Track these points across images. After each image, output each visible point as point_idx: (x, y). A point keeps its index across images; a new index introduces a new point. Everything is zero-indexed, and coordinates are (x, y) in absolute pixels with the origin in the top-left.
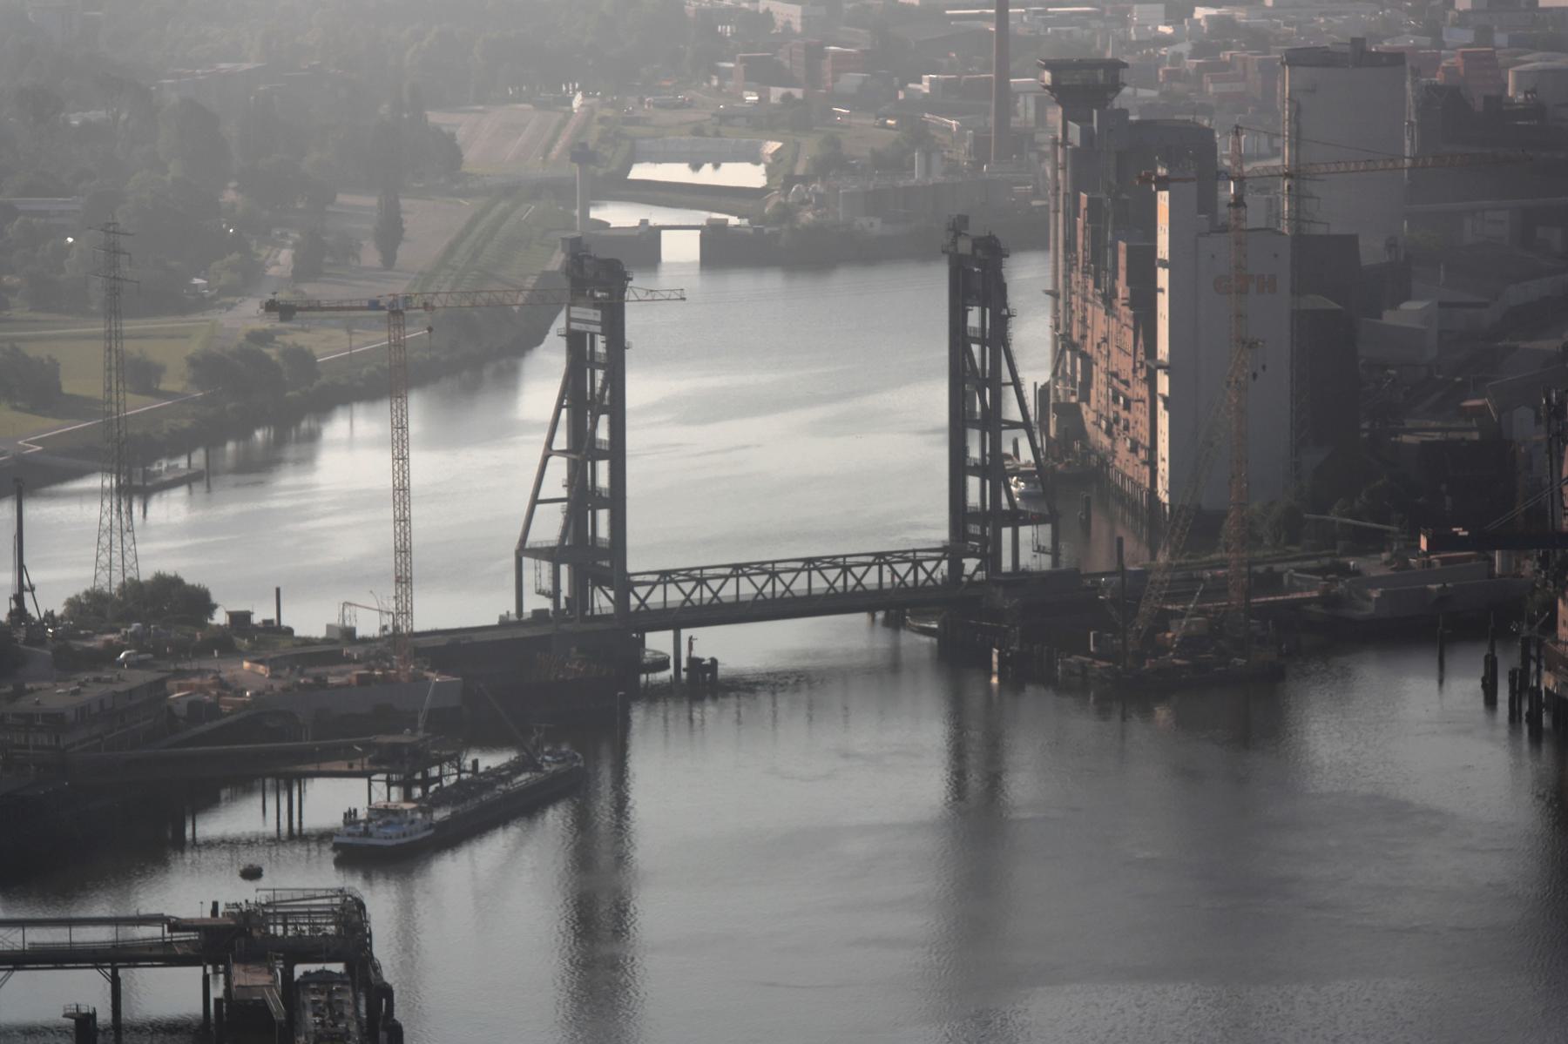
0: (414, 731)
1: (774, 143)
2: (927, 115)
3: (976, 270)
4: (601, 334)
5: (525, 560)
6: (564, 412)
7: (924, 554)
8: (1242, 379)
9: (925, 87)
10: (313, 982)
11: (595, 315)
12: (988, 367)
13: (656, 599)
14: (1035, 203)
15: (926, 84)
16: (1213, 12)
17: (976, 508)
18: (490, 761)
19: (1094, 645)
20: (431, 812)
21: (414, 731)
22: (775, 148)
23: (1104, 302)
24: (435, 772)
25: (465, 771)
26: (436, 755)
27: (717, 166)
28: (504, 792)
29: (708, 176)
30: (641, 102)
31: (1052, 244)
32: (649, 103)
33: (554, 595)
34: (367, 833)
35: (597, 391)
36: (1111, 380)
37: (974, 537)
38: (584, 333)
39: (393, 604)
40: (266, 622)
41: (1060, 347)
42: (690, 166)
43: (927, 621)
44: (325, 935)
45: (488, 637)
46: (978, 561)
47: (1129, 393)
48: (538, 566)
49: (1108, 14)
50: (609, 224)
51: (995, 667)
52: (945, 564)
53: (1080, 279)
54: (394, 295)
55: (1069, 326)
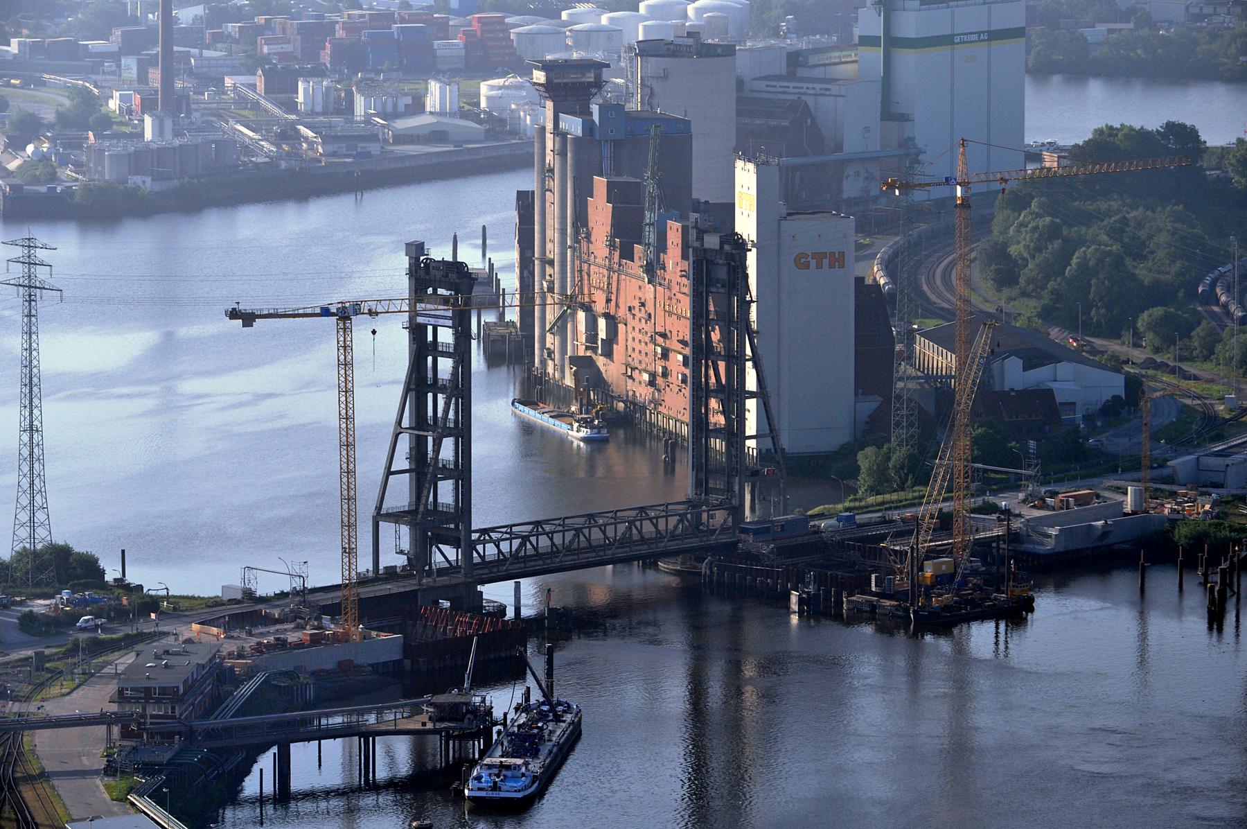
2: (46, 76)
5: (383, 525)
19: (876, 586)
40: (116, 580)
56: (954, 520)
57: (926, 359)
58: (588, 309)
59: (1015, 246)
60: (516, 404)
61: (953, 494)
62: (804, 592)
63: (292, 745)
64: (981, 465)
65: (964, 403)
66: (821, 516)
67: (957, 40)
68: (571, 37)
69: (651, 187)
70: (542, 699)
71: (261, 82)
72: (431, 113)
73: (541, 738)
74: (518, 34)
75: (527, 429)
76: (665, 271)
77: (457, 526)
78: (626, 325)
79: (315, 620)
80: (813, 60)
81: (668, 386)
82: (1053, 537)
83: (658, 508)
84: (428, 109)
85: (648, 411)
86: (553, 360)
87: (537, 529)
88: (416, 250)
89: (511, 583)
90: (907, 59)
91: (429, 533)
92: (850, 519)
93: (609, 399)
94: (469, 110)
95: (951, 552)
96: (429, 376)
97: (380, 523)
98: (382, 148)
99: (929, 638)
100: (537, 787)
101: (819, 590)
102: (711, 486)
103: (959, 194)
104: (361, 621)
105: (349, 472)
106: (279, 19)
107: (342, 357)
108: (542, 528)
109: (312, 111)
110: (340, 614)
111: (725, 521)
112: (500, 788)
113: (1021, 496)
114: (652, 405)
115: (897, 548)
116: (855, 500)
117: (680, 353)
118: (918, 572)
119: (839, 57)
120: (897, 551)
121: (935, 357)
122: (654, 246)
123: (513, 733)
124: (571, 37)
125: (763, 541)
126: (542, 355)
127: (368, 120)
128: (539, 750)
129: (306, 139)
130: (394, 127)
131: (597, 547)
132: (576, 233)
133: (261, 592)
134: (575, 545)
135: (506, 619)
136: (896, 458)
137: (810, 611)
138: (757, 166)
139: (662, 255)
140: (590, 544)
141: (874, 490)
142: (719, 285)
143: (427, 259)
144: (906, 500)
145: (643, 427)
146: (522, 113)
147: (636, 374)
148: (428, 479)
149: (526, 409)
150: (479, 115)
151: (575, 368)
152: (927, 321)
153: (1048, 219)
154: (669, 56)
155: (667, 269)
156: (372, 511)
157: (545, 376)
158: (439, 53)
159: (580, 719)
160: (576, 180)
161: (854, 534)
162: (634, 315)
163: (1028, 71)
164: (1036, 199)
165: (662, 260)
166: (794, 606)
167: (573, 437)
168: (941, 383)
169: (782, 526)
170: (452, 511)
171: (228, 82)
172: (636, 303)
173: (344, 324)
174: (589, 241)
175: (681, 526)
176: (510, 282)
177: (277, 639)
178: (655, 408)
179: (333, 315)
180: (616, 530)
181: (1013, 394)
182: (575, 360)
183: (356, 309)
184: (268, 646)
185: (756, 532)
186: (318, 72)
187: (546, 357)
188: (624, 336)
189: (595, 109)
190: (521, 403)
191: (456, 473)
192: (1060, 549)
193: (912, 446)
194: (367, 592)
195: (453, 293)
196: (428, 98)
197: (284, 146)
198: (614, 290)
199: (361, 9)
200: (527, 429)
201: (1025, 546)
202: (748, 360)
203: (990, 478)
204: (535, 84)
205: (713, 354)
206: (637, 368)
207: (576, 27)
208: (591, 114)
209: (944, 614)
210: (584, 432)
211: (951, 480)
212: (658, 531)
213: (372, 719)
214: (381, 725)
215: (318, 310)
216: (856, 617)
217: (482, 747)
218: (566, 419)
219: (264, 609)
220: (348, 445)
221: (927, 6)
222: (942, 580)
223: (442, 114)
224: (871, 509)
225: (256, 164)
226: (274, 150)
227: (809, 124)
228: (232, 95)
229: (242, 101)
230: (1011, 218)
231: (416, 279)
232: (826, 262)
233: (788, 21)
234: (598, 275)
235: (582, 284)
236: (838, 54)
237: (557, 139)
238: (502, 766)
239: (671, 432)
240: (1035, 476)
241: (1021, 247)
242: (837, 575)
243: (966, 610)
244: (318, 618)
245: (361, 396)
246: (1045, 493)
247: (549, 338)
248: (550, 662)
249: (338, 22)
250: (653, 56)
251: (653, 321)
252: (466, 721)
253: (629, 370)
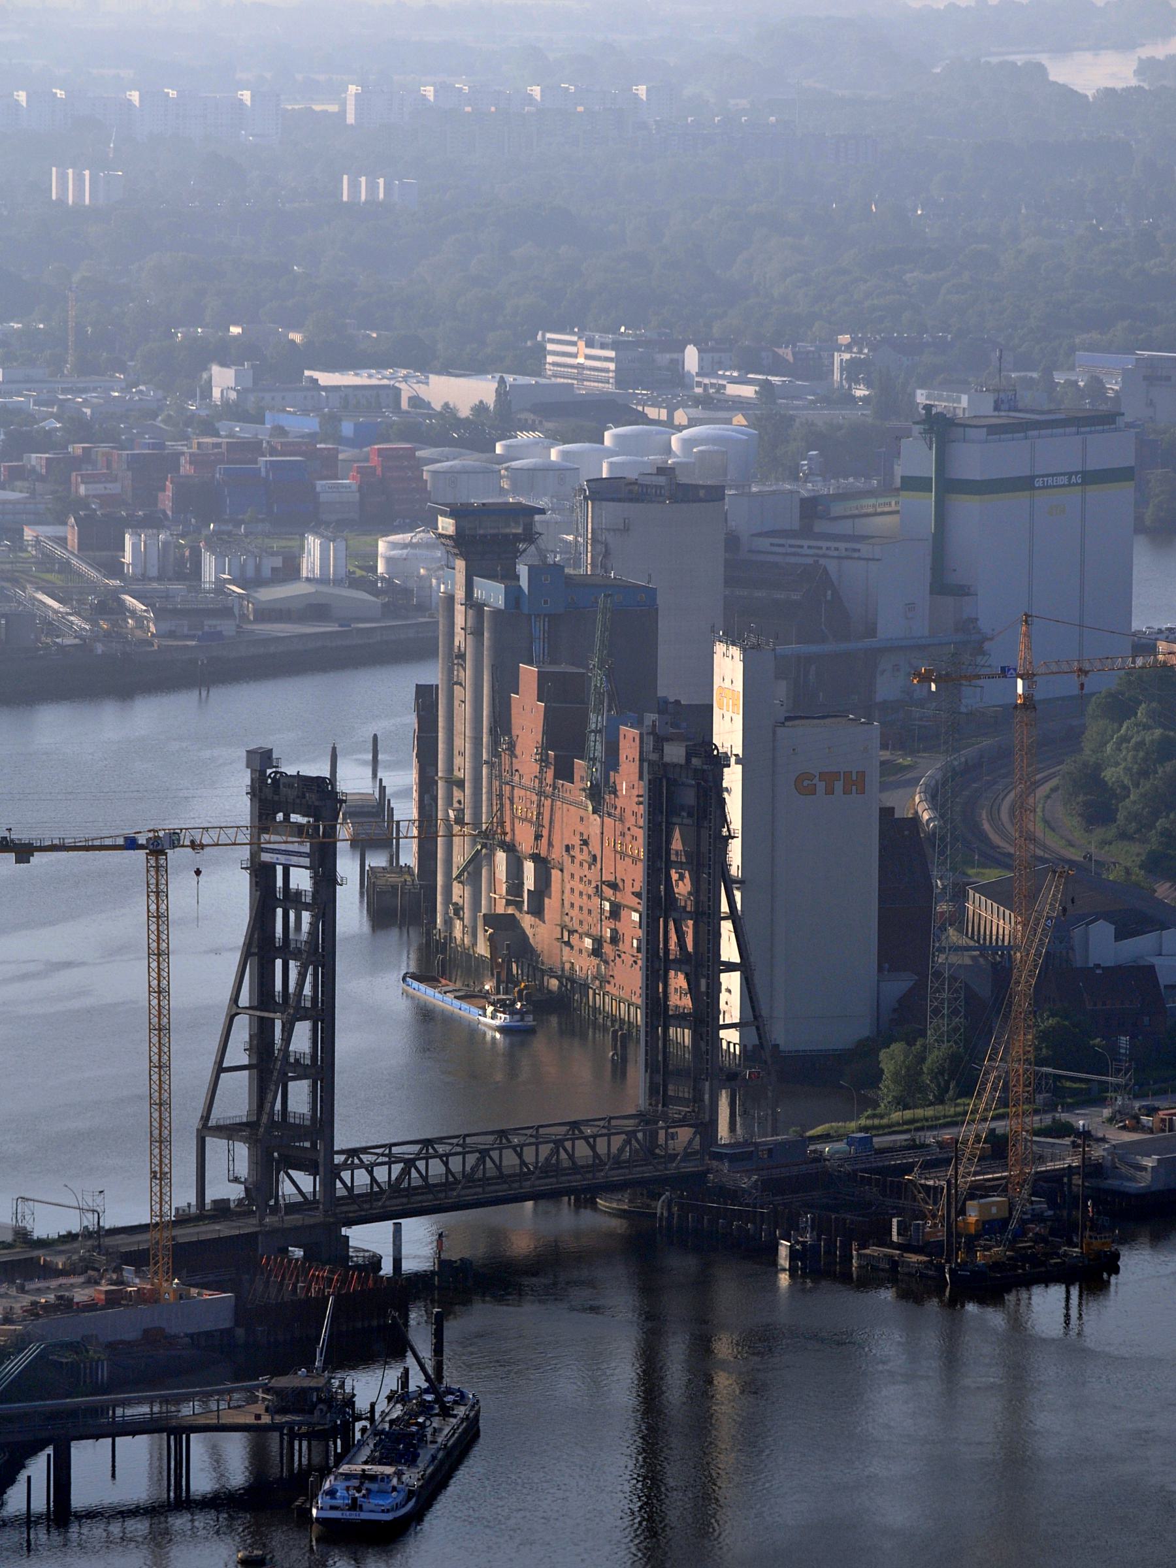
19: (899, 1234)
48: (231, 1148)
56: (1010, 1144)
57: (982, 922)
58: (510, 848)
59: (1113, 769)
60: (408, 979)
61: (1009, 1110)
62: (798, 1242)
63: (73, 1444)
64: (1049, 1070)
65: (1024, 982)
66: (826, 1138)
67: (1038, 483)
68: (507, 477)
69: (598, 680)
70: (425, 1385)
71: (73, 533)
72: (308, 579)
73: (422, 1437)
74: (434, 472)
75: (426, 1015)
76: (616, 796)
77: (314, 1145)
78: (562, 870)
79: (114, 1272)
80: (837, 509)
81: (619, 956)
82: (1149, 1169)
83: (596, 1123)
84: (304, 574)
85: (591, 992)
86: (462, 919)
87: (427, 1150)
88: (261, 760)
89: (388, 1225)
90: (967, 508)
91: (276, 1154)
92: (866, 1142)
93: (538, 974)
94: (363, 578)
95: (1005, 1189)
96: (277, 935)
97: (207, 1138)
98: (238, 626)
99: (971, 1308)
100: (413, 1508)
101: (819, 1240)
102: (670, 1093)
103: (1020, 690)
104: (176, 1274)
105: (161, 1066)
106: (104, 448)
107: (153, 907)
108: (433, 1148)
109: (143, 575)
110: (148, 1265)
111: (690, 1142)
112: (361, 1506)
113: (1107, 1112)
114: (597, 982)
115: (931, 1183)
116: (874, 1116)
117: (636, 911)
118: (957, 1216)
119: (874, 506)
120: (929, 1186)
121: (995, 921)
122: (601, 762)
123: (383, 1432)
124: (507, 477)
125: (743, 1171)
126: (447, 913)
127: (220, 584)
128: (418, 1455)
129: (133, 613)
130: (255, 598)
131: (510, 1176)
132: (495, 743)
133: (40, 1231)
134: (479, 1174)
135: (382, 1273)
136: (934, 1057)
137: (806, 1269)
138: (744, 650)
139: (612, 773)
140: (501, 1172)
141: (902, 1103)
143: (276, 773)
144: (945, 1117)
145: (584, 1013)
146: (434, 581)
147: (575, 939)
148: (274, 1078)
149: (422, 987)
150: (376, 582)
151: (491, 931)
152: (987, 871)
153: (1158, 732)
154: (631, 500)
155: (618, 793)
156: (195, 1123)
157: (451, 942)
158: (323, 498)
159: (478, 1412)
160: (494, 669)
161: (871, 1162)
162: (573, 857)
163: (1140, 528)
164: (1143, 705)
165: (612, 780)
166: (784, 1260)
167: (486, 1025)
168: (1002, 956)
169: (770, 1151)
170: (307, 1123)
171: (29, 534)
172: (576, 841)
173: (157, 860)
174: (513, 755)
175: (628, 1149)
176: (406, 810)
177: (60, 1298)
178: (601, 987)
179: (142, 847)
180: (537, 1155)
181: (1099, 971)
182: (492, 920)
183: (175, 839)
184: (47, 1307)
185: (732, 1158)
186: (153, 522)
187: (452, 915)
188: (559, 886)
189: (523, 571)
190: (415, 977)
191: (313, 1071)
192: (1159, 1186)
193: (956, 1042)
194: (187, 1234)
195: (311, 820)
196: (305, 560)
197: (101, 622)
198: (546, 822)
199: (219, 436)
200: (426, 1015)
201: (1109, 1182)
202: (725, 918)
203: (1064, 1087)
204: (441, 536)
205: (675, 910)
206: (576, 931)
207: (516, 464)
208: (517, 578)
209: (993, 1275)
210: (502, 1019)
211: (1006, 1088)
212: (596, 1155)
213: (186, 1410)
214: (198, 1417)
215: (121, 841)
216: (869, 1280)
217: (339, 1450)
218: (476, 1001)
219: (43, 1256)
220: (161, 1029)
221: (1010, 436)
222: (992, 1227)
223: (323, 580)
224: (896, 1129)
225: (61, 647)
226: (87, 627)
227: (829, 598)
228: (34, 553)
229: (47, 561)
230: (1109, 732)
231: (260, 800)
232: (839, 786)
233: (810, 459)
234: (524, 802)
235: (502, 814)
236: (872, 501)
237: (470, 612)
238: (365, 1477)
239: (622, 1021)
240: (1127, 1085)
241: (1120, 769)
242: (844, 1220)
243: (1024, 1270)
244: (118, 1270)
245: (180, 968)
246: (1139, 1109)
247: (457, 889)
248: (439, 1335)
249: (183, 454)
250: (613, 500)
251: (599, 866)
252: (317, 1413)
253: (566, 934)
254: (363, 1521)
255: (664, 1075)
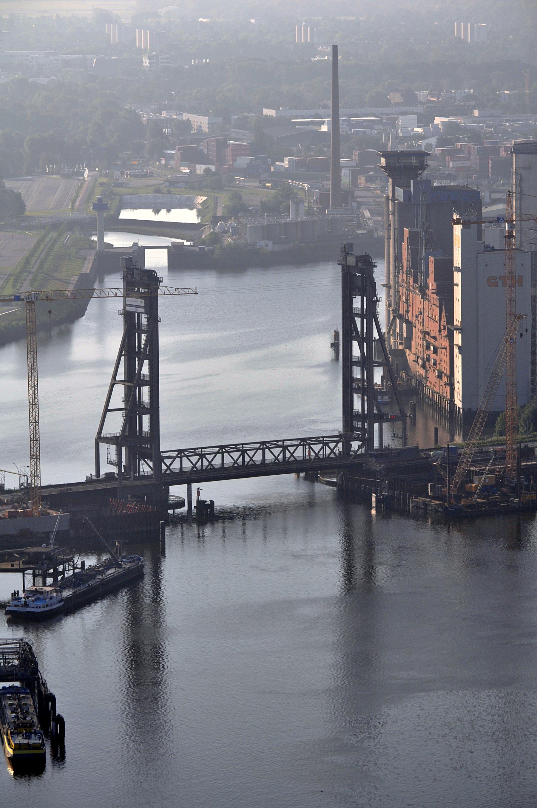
0: (48, 545)
1: (202, 197)
2: (289, 181)
3: (357, 274)
4: (144, 313)
5: (103, 446)
6: (123, 358)
7: (330, 439)
8: (514, 337)
9: (286, 164)
10: (9, 693)
11: (141, 302)
12: (365, 331)
13: (176, 466)
14: (359, 232)
15: (286, 162)
16: (446, 120)
17: (358, 412)
18: (91, 561)
19: (431, 491)
20: (61, 592)
21: (48, 545)
22: (203, 200)
23: (421, 291)
24: (60, 568)
25: (77, 568)
26: (61, 558)
27: (169, 211)
28: (102, 580)
29: (163, 216)
30: (122, 173)
31: (385, 256)
32: (127, 175)
33: (118, 464)
34: (26, 605)
35: (142, 346)
36: (425, 336)
37: (358, 429)
38: (134, 313)
39: (28, 470)
41: (392, 317)
42: (153, 211)
43: (330, 477)
44: (12, 665)
45: (81, 489)
46: (360, 443)
47: (436, 344)
48: (109, 448)
49: (384, 121)
50: (113, 245)
51: (374, 505)
52: (340, 445)
53: (405, 278)
54: (29, 292)
55: (397, 304)
142: (357, 290)
179: (23, 300)
215: (13, 297)
243: (485, 508)
250: (524, 153)
254: (27, 612)
255: (351, 417)
